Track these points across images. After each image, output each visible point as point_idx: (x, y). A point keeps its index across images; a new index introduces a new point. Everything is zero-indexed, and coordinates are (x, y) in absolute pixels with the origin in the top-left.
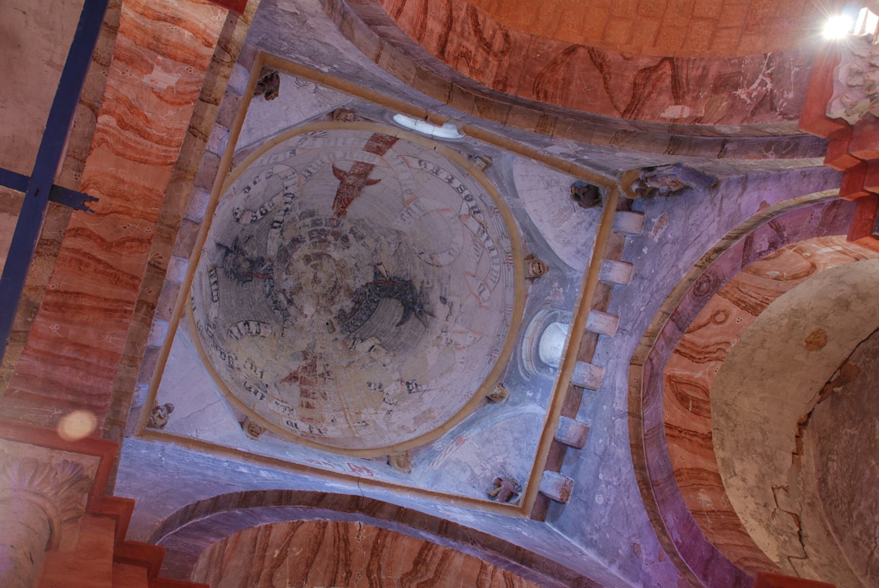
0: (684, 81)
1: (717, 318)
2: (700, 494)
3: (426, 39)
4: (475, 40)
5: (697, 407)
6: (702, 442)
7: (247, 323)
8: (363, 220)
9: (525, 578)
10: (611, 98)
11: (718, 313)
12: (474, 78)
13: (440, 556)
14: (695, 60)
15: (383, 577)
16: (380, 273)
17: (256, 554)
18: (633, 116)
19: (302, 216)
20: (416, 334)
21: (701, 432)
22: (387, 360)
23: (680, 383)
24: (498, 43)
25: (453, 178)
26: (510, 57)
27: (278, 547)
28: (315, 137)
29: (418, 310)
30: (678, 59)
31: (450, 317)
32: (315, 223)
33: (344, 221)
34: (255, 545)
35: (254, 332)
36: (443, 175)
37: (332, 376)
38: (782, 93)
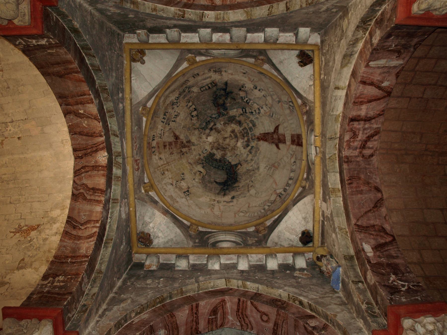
0: (386, 249)
1: (264, 316)
2: (164, 330)
3: (356, 107)
4: (364, 138)
5: (212, 322)
6: (194, 328)
7: (195, 109)
8: (259, 150)
9: (96, 243)
10: (362, 216)
11: (267, 315)
12: (345, 144)
13: (99, 199)
14: (399, 251)
15: (83, 175)
16: (237, 167)
17: (78, 98)
18: (357, 230)
19: (252, 122)
20: (213, 190)
21: (199, 326)
22: (197, 180)
23: (223, 308)
24: (367, 152)
25: (292, 179)
26: (362, 160)
27: (85, 112)
28: (289, 108)
29: (225, 188)
30: (396, 243)
31: (226, 203)
32: (250, 129)
33: (256, 142)
34: (82, 96)
35: (193, 114)
36: (292, 175)
37: (182, 156)
38: (403, 296)
